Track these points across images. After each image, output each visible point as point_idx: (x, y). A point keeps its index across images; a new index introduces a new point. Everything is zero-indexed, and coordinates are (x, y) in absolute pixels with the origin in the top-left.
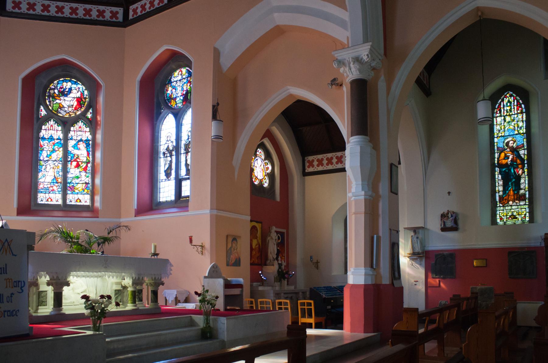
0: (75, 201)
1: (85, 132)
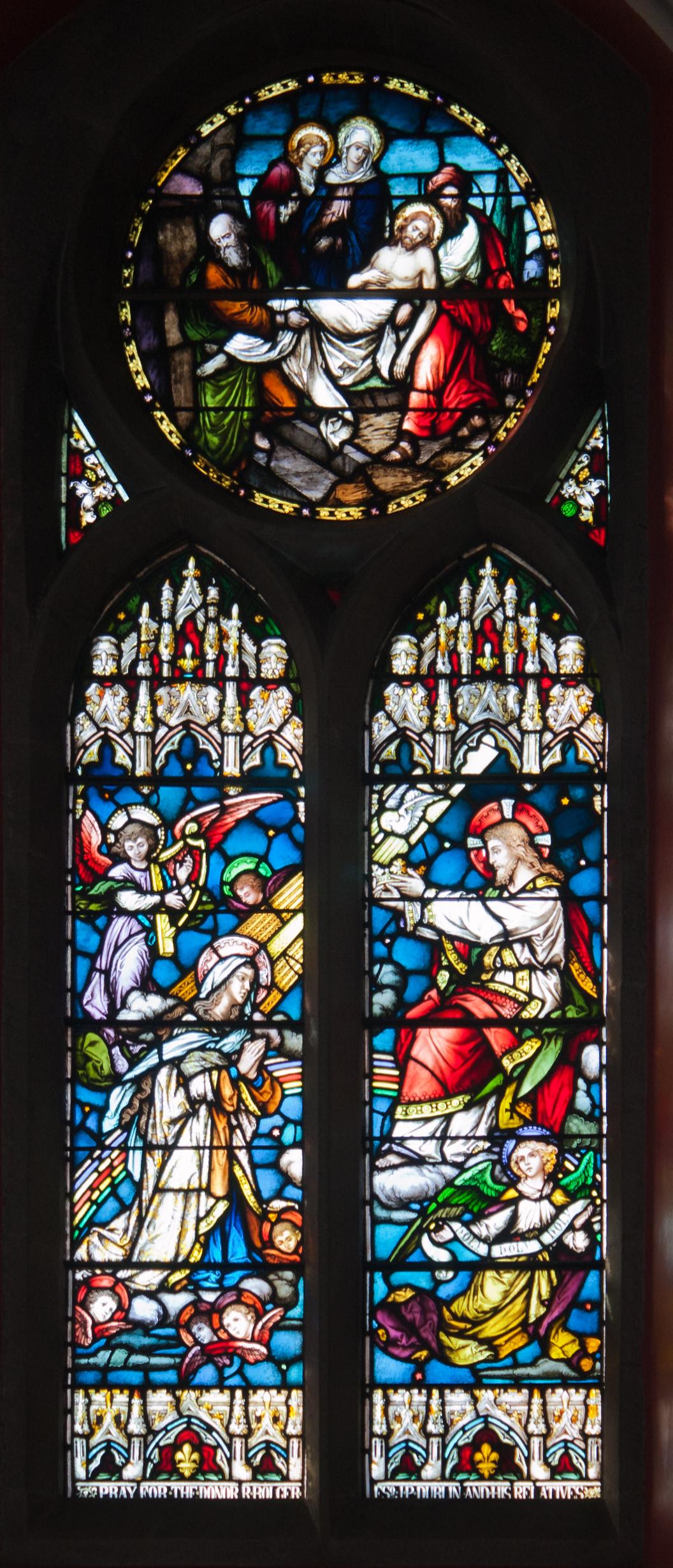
1: (546, 679)
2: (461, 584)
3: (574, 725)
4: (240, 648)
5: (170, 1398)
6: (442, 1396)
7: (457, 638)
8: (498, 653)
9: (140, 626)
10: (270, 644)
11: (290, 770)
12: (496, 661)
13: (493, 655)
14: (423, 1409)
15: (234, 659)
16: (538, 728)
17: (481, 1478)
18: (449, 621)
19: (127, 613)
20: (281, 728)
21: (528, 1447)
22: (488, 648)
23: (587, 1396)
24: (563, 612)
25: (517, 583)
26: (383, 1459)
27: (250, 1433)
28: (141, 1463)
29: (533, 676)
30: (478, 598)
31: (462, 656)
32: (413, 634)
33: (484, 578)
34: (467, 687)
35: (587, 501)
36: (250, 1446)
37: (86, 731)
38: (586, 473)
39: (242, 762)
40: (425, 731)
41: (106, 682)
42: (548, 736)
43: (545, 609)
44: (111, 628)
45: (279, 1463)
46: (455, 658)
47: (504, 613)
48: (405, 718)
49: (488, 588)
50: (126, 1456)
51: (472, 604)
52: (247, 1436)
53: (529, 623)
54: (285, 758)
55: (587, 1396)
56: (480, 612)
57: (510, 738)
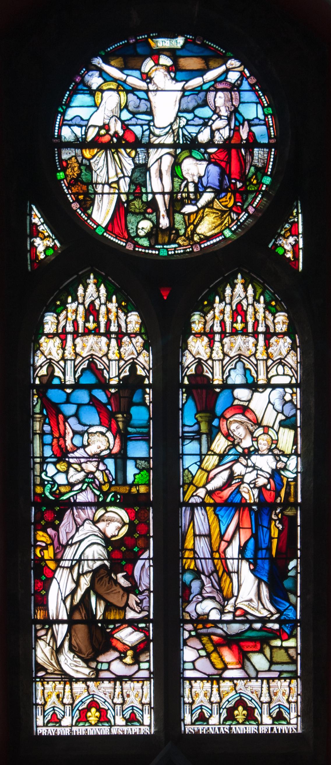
0: (224, 714)
1: (120, 335)
2: (78, 286)
3: (134, 357)
8: (245, 321)
10: (280, 315)
12: (95, 325)
13: (94, 322)
15: (114, 322)
16: (117, 358)
17: (238, 723)
20: (286, 357)
23: (290, 683)
24: (55, 300)
25: (254, 287)
26: (190, 715)
31: (249, 323)
32: (54, 312)
34: (229, 338)
36: (124, 709)
37: (188, 360)
41: (198, 335)
43: (268, 299)
44: (53, 309)
45: (286, 715)
47: (100, 301)
48: (50, 353)
49: (92, 288)
51: (232, 297)
52: (269, 703)
53: (260, 307)
54: (140, 372)
55: (290, 683)
56: (235, 301)
57: (251, 363)
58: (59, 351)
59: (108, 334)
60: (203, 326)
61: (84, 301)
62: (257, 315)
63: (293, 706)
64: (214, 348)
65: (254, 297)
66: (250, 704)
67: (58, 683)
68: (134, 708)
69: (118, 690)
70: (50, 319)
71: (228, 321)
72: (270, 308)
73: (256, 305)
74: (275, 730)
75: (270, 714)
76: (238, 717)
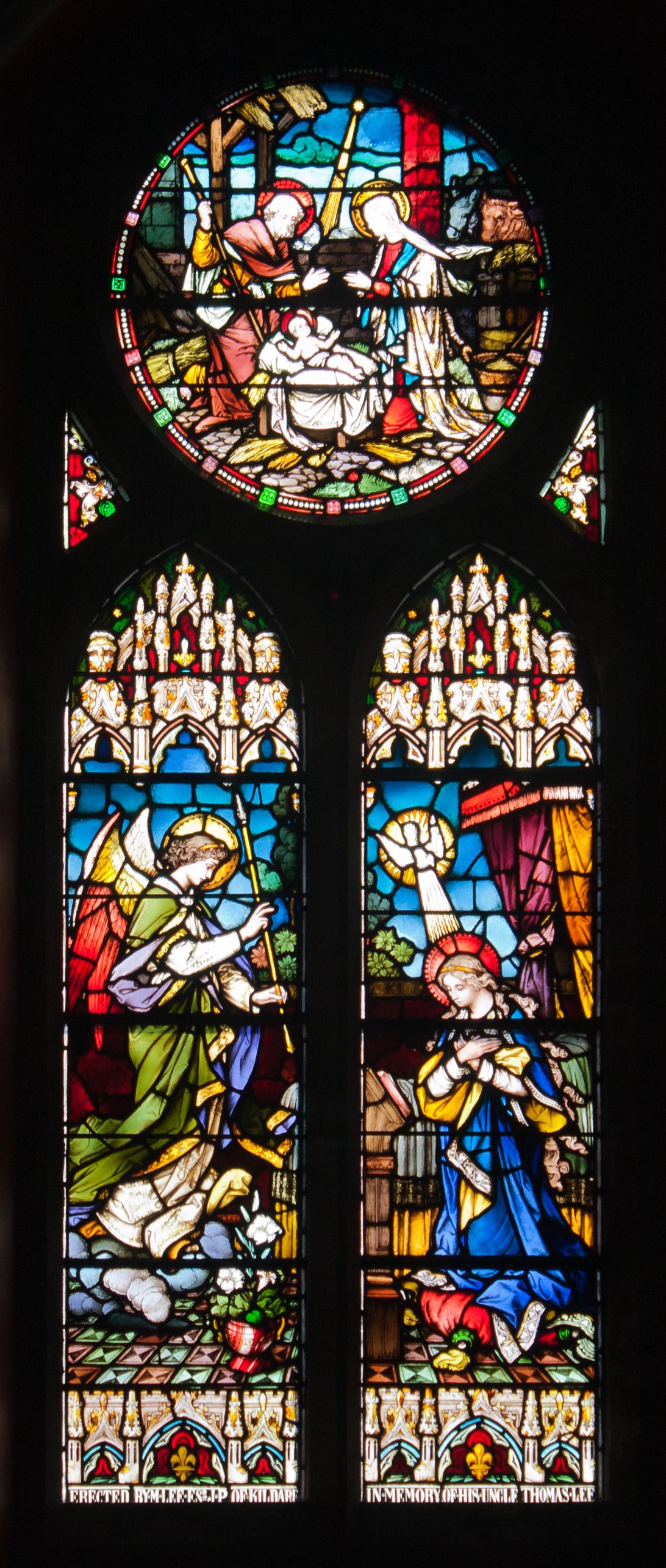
0: (446, 1461)
1: (536, 677)
3: (566, 721)
4: (235, 642)
5: (164, 1399)
6: (138, 1398)
7: (154, 634)
8: (489, 650)
9: (136, 622)
10: (263, 638)
11: (288, 763)
13: (190, 651)
14: (416, 1408)
15: (230, 652)
18: (441, 619)
19: (122, 609)
21: (522, 1450)
22: (185, 644)
25: (506, 580)
27: (246, 1435)
28: (137, 1466)
29: (229, 673)
30: (175, 594)
31: (454, 653)
32: (404, 631)
33: (181, 574)
35: (578, 498)
37: (375, 728)
38: (577, 471)
39: (240, 757)
40: (418, 728)
41: (100, 678)
42: (540, 733)
46: (151, 652)
49: (184, 583)
50: (122, 1459)
58: (415, 711)
59: (512, 676)
60: (407, 662)
61: (169, 608)
62: (220, 638)
63: (428, 1445)
64: (430, 704)
65: (509, 601)
66: (202, 1442)
67: (272, 1393)
68: (403, 1445)
69: (131, 1411)
70: (99, 643)
71: (162, 648)
72: (542, 623)
73: (218, 616)
74: (171, 1496)
75: (540, 1460)
76: (474, 1467)
